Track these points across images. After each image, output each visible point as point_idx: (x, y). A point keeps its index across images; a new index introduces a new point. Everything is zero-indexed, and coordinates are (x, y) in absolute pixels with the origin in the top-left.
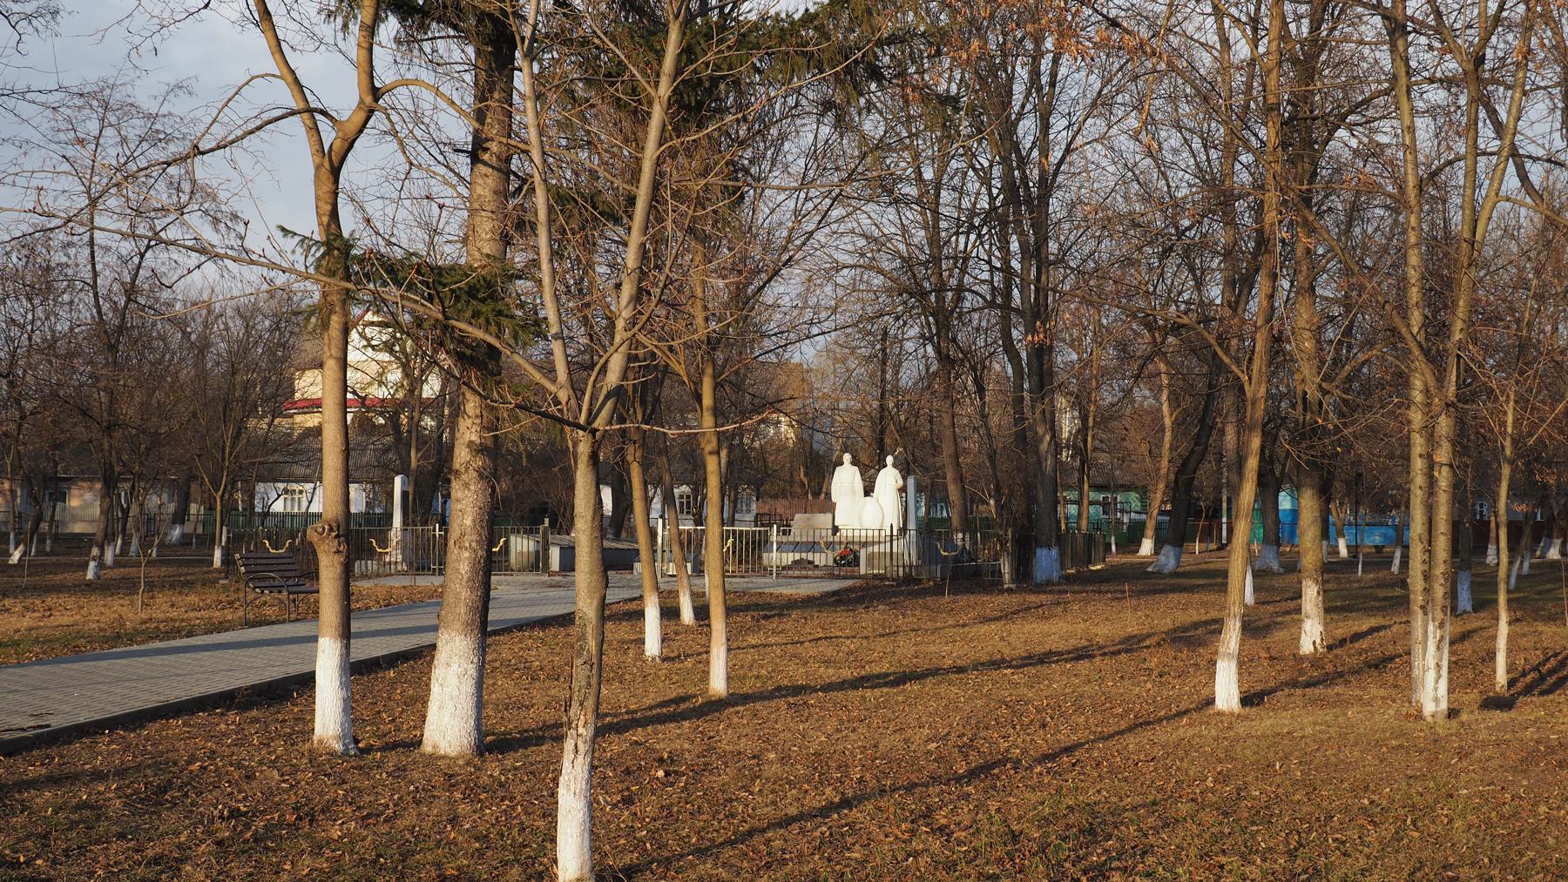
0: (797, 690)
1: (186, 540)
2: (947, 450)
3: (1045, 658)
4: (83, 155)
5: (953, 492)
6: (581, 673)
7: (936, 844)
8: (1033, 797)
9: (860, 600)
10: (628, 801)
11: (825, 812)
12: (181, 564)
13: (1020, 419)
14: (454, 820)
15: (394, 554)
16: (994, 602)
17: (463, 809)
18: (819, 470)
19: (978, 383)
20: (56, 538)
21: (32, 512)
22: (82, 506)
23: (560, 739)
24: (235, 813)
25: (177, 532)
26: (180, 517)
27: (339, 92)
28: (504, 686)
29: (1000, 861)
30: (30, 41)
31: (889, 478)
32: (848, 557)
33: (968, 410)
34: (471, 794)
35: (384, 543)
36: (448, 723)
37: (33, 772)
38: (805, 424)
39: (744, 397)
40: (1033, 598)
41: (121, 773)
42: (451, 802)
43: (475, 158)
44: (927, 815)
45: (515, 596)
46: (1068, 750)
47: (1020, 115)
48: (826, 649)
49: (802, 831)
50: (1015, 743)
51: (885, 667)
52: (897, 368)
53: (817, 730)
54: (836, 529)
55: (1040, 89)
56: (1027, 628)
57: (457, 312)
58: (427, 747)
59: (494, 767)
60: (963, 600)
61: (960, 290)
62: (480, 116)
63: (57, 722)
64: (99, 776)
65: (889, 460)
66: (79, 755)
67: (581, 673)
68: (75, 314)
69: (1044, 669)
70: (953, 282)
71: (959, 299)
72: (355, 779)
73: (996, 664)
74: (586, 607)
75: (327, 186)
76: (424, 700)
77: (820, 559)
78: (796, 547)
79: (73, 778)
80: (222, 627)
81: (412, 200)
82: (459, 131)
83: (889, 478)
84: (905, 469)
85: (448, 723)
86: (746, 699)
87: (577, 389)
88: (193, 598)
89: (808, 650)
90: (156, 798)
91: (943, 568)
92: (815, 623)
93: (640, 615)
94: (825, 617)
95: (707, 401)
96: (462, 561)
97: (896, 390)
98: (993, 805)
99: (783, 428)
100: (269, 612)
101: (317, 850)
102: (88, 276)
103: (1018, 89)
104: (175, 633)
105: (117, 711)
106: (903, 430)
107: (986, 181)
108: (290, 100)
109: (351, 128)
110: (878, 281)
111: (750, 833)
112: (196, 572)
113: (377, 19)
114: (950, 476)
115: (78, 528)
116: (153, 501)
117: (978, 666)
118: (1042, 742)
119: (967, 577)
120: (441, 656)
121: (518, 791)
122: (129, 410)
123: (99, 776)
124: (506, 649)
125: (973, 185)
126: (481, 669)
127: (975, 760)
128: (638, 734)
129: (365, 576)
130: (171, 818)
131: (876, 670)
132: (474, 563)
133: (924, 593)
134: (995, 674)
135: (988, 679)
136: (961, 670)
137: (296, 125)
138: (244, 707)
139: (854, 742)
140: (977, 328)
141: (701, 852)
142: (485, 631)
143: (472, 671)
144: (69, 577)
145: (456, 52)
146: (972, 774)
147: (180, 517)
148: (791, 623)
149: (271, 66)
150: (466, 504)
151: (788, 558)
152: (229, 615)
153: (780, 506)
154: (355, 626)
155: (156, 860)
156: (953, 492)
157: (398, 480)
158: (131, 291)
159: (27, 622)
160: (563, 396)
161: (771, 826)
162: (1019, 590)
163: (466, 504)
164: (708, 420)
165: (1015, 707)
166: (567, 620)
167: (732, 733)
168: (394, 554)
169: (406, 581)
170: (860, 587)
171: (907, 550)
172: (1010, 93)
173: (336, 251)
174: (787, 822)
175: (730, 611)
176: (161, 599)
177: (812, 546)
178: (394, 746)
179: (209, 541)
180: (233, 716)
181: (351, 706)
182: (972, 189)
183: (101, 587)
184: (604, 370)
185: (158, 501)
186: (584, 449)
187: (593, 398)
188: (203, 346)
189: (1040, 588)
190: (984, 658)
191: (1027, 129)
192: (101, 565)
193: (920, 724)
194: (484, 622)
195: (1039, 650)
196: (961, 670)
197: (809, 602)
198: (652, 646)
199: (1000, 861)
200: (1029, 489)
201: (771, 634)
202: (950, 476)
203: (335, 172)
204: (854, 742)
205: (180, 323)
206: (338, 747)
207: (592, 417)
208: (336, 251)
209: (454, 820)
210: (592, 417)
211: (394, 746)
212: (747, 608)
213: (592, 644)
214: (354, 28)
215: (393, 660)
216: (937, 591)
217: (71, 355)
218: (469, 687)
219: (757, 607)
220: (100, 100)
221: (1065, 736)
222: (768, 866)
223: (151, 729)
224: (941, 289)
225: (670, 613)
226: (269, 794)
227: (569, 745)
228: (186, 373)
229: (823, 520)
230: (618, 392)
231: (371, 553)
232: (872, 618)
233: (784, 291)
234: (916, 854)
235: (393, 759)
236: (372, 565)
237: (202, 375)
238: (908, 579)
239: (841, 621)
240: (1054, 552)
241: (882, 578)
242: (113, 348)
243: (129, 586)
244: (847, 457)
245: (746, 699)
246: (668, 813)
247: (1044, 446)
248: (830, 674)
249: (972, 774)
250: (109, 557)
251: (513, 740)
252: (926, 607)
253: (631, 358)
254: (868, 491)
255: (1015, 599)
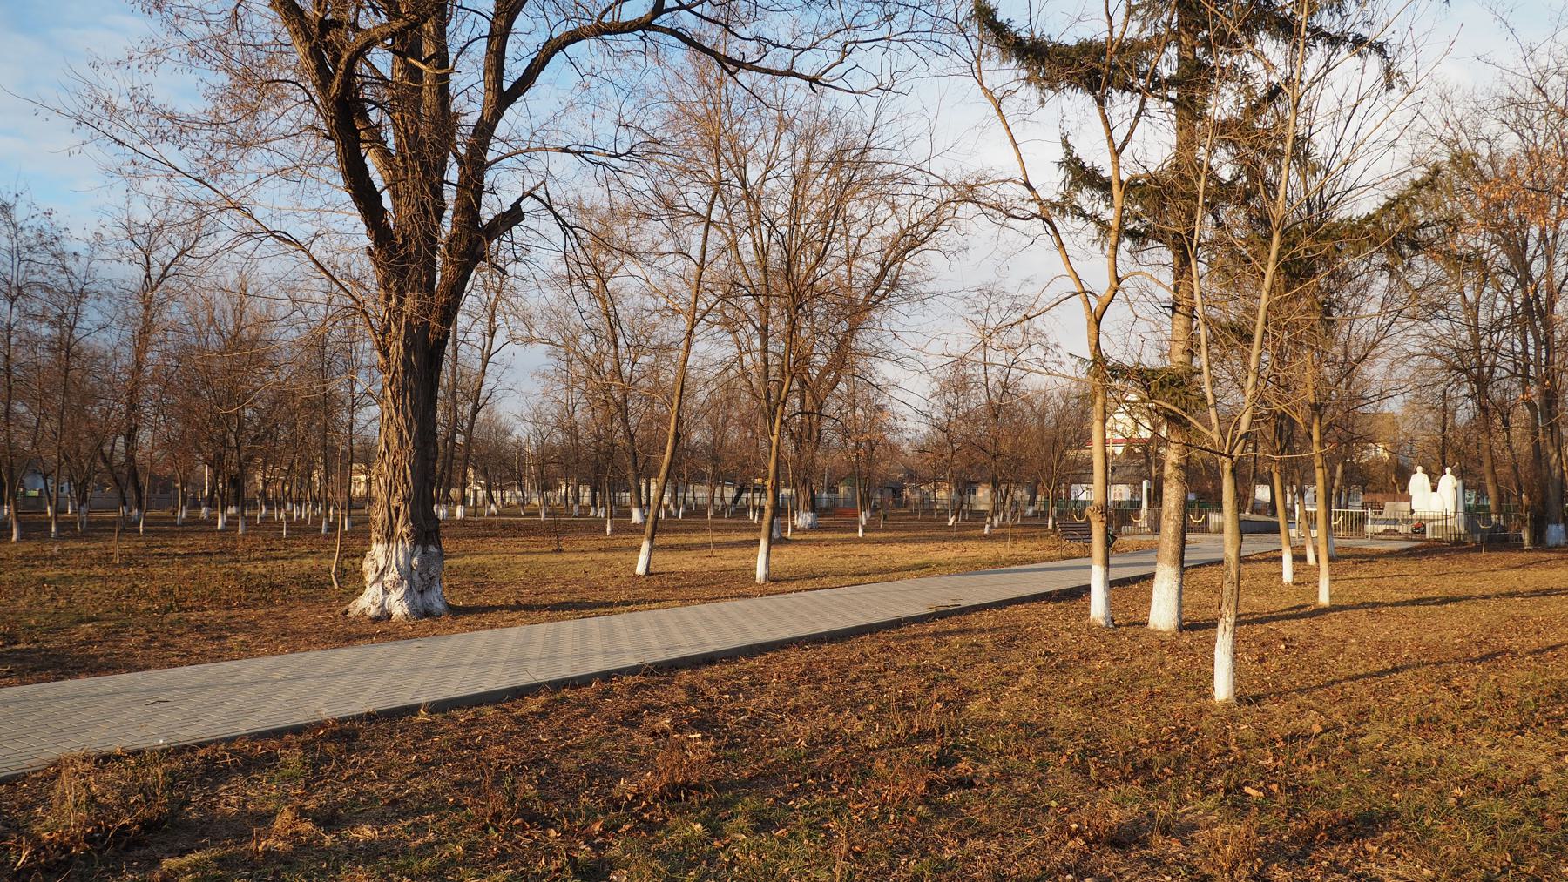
0: (1375, 605)
1: (1035, 514)
2: (1487, 464)
3: (1547, 593)
4: (980, 319)
5: (1491, 489)
6: (1227, 588)
7: (1449, 697)
8: (1520, 674)
9: (1424, 554)
10: (1262, 660)
11: (1380, 674)
12: (1032, 526)
13: (1536, 446)
14: (1162, 664)
15: (1143, 523)
16: (1517, 557)
17: (1167, 659)
18: (1404, 475)
19: (1506, 423)
20: (971, 512)
21: (958, 499)
22: (983, 497)
23: (1215, 625)
24: (1048, 653)
25: (1030, 510)
26: (1032, 502)
27: (1100, 282)
28: (1199, 596)
29: (1490, 709)
30: (955, 264)
31: (1448, 481)
32: (1420, 528)
33: (1501, 438)
34: (1173, 651)
35: (1138, 517)
36: (1162, 612)
37: (952, 627)
38: (1396, 449)
39: (1347, 432)
40: (1545, 555)
41: (992, 630)
42: (1162, 655)
43: (1174, 310)
44: (1448, 679)
45: (1201, 547)
46: (1553, 648)
47: (1533, 258)
48: (1397, 582)
49: (1365, 684)
50: (1516, 642)
51: (1436, 593)
52: (1453, 414)
53: (1386, 628)
54: (1412, 512)
55: (1546, 241)
56: (1539, 573)
57: (1170, 391)
58: (1151, 626)
59: (1186, 638)
60: (1494, 555)
61: (1493, 366)
62: (1176, 289)
63: (964, 604)
64: (982, 631)
65: (1448, 470)
66: (974, 620)
67: (1227, 588)
68: (977, 400)
69: (1546, 599)
70: (1488, 362)
71: (1492, 372)
72: (1110, 640)
73: (1511, 595)
74: (1230, 553)
75: (1094, 330)
76: (1149, 600)
77: (1403, 529)
78: (1386, 521)
79: (970, 631)
80: (1050, 559)
81: (1142, 334)
82: (1166, 295)
83: (1448, 481)
84: (1460, 474)
85: (1162, 612)
86: (1341, 608)
87: (1223, 433)
88: (1036, 544)
89: (1386, 582)
90: (1009, 643)
91: (1482, 535)
92: (1393, 566)
93: (1280, 559)
94: (1401, 563)
95: (1316, 437)
96: (1170, 526)
97: (1454, 427)
98: (1492, 677)
99: (1380, 451)
100: (1075, 552)
101: (1088, 674)
102: (983, 380)
103: (1532, 244)
104: (1026, 562)
105: (993, 600)
106: (1458, 453)
107: (1510, 299)
108: (1076, 289)
109: (1106, 300)
110: (1437, 363)
111: (1333, 682)
112: (1038, 531)
113: (1118, 241)
114: (1488, 479)
115: (982, 508)
116: (1018, 494)
117: (1499, 595)
118: (1534, 642)
119: (1499, 541)
120: (1158, 578)
121: (1199, 652)
122: (1005, 447)
123: (982, 631)
124: (1191, 578)
125: (1501, 303)
126: (1181, 585)
127: (1486, 650)
128: (1273, 625)
129: (1127, 534)
130: (1016, 653)
131: (1430, 595)
132: (1176, 528)
133: (1469, 550)
134: (1509, 600)
135: (1503, 605)
136: (1486, 597)
137: (1078, 300)
138: (1057, 600)
139: (1406, 636)
140: (1505, 386)
141: (1301, 691)
142: (1183, 568)
143: (1176, 586)
144: (976, 532)
145: (1167, 256)
146: (1482, 658)
147: (1032, 502)
148: (1377, 567)
149: (1064, 270)
150: (1172, 495)
151: (1381, 528)
152: (1053, 553)
153: (1379, 497)
154: (1111, 561)
155: (1007, 674)
156: (1491, 489)
157: (1145, 483)
158: (1005, 387)
159: (954, 554)
160: (1216, 437)
161: (1347, 679)
162: (1535, 550)
163: (1172, 495)
164: (1316, 448)
165: (1520, 621)
166: (1221, 562)
167: (1329, 628)
168: (1143, 523)
169: (1150, 537)
170: (1425, 547)
171: (1458, 525)
172: (1526, 245)
173: (1099, 360)
174: (1356, 678)
175: (1331, 559)
176: (1020, 544)
177: (1396, 522)
178: (1134, 624)
179: (1045, 515)
180: (1050, 605)
181: (1111, 603)
182: (1498, 303)
183: (991, 538)
184: (1238, 423)
185: (1021, 494)
186: (1227, 466)
187: (1232, 440)
188: (1041, 416)
189: (1550, 549)
190: (1504, 591)
191: (1537, 268)
192: (992, 527)
193: (1453, 628)
194: (1182, 561)
195: (1545, 587)
196: (1486, 597)
197: (1391, 554)
198: (1288, 576)
199: (1490, 709)
200: (1544, 489)
201: (1364, 572)
202: (1488, 479)
203: (1098, 323)
204: (1406, 636)
205: (1029, 401)
206: (1103, 623)
207: (1231, 450)
208: (1099, 360)
209: (1162, 664)
210: (1231, 450)
211: (1134, 624)
212: (1349, 557)
213: (1234, 572)
214: (1106, 248)
215: (1137, 579)
216: (1478, 549)
217: (976, 420)
218: (1174, 594)
219: (1356, 556)
220: (987, 291)
221: (1552, 639)
222: (1341, 701)
223: (1010, 608)
224: (1481, 365)
225: (1299, 558)
226: (1066, 645)
227: (1221, 626)
228: (1034, 427)
229: (1404, 506)
230: (1246, 436)
231: (1130, 522)
232: (1430, 565)
233: (1375, 371)
234: (1434, 701)
235: (1132, 631)
236: (1131, 529)
237: (1042, 428)
238: (1458, 542)
239: (1411, 566)
240: (1561, 527)
241: (1441, 541)
242: (996, 416)
243: (1003, 537)
244: (1419, 469)
245: (1341, 608)
246: (1285, 669)
247: (1553, 461)
248: (1398, 596)
249: (1482, 658)
250: (996, 523)
251: (1195, 625)
252: (1468, 559)
253: (1253, 417)
254: (1434, 489)
255: (1530, 555)
